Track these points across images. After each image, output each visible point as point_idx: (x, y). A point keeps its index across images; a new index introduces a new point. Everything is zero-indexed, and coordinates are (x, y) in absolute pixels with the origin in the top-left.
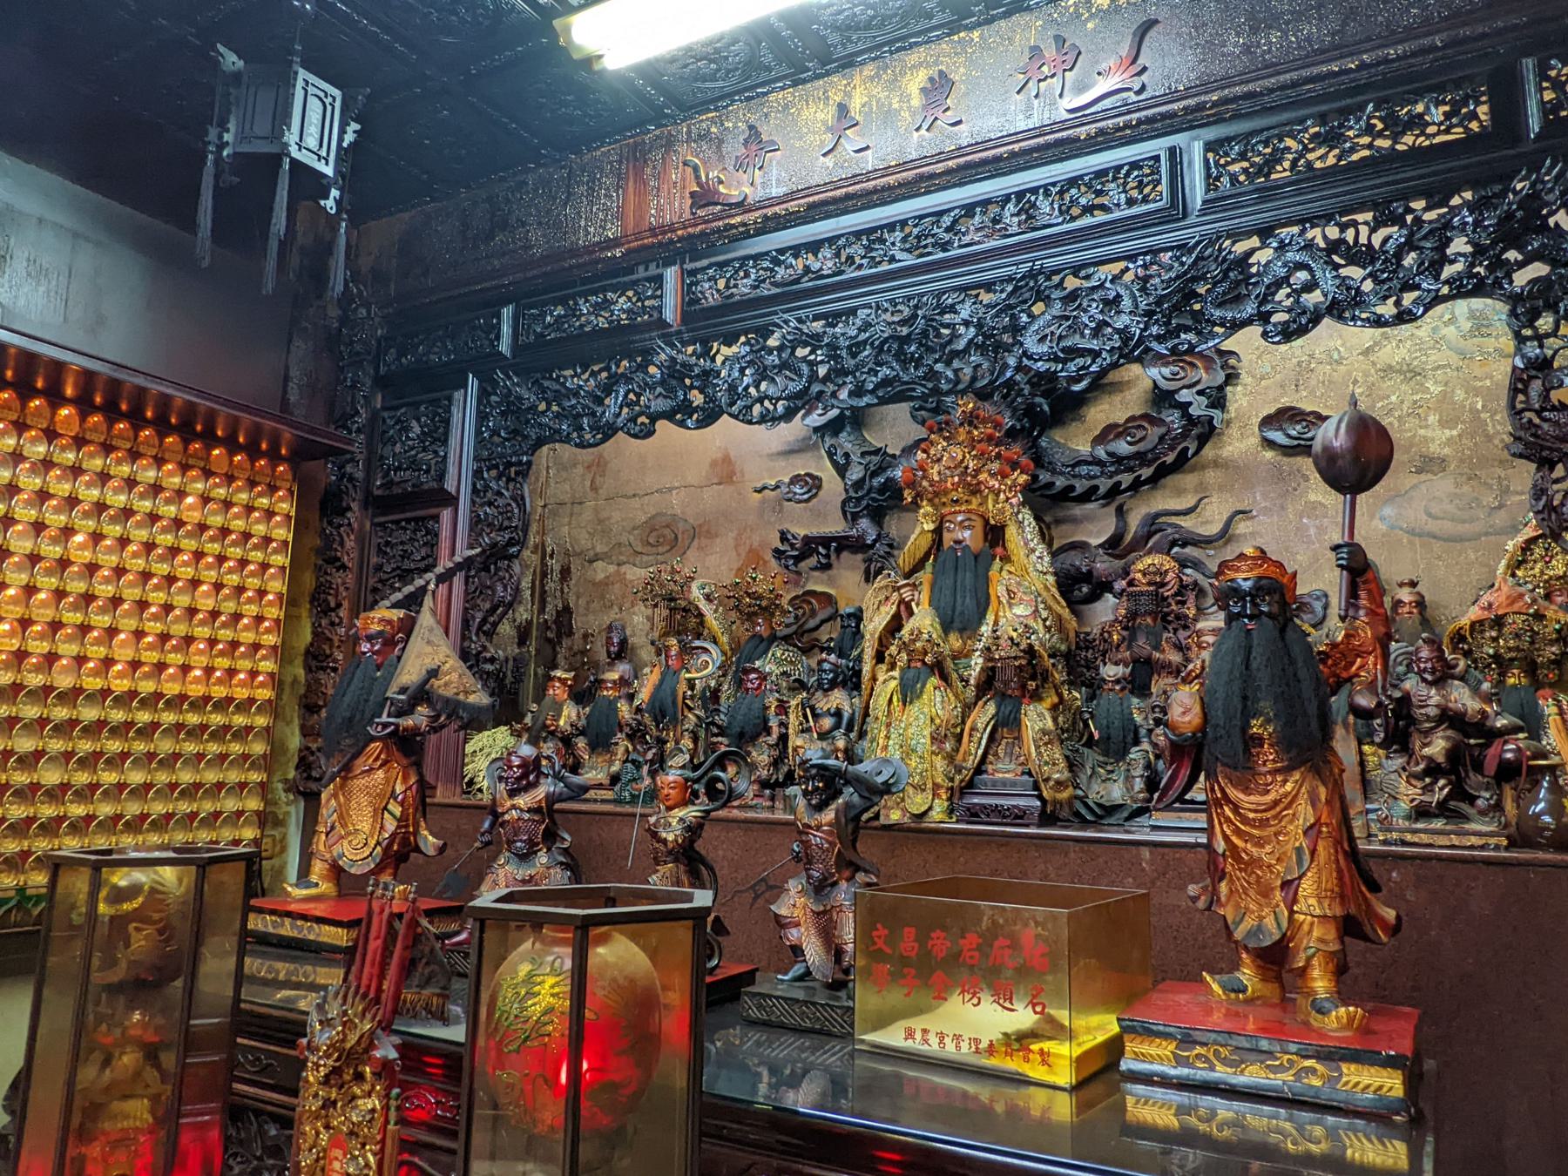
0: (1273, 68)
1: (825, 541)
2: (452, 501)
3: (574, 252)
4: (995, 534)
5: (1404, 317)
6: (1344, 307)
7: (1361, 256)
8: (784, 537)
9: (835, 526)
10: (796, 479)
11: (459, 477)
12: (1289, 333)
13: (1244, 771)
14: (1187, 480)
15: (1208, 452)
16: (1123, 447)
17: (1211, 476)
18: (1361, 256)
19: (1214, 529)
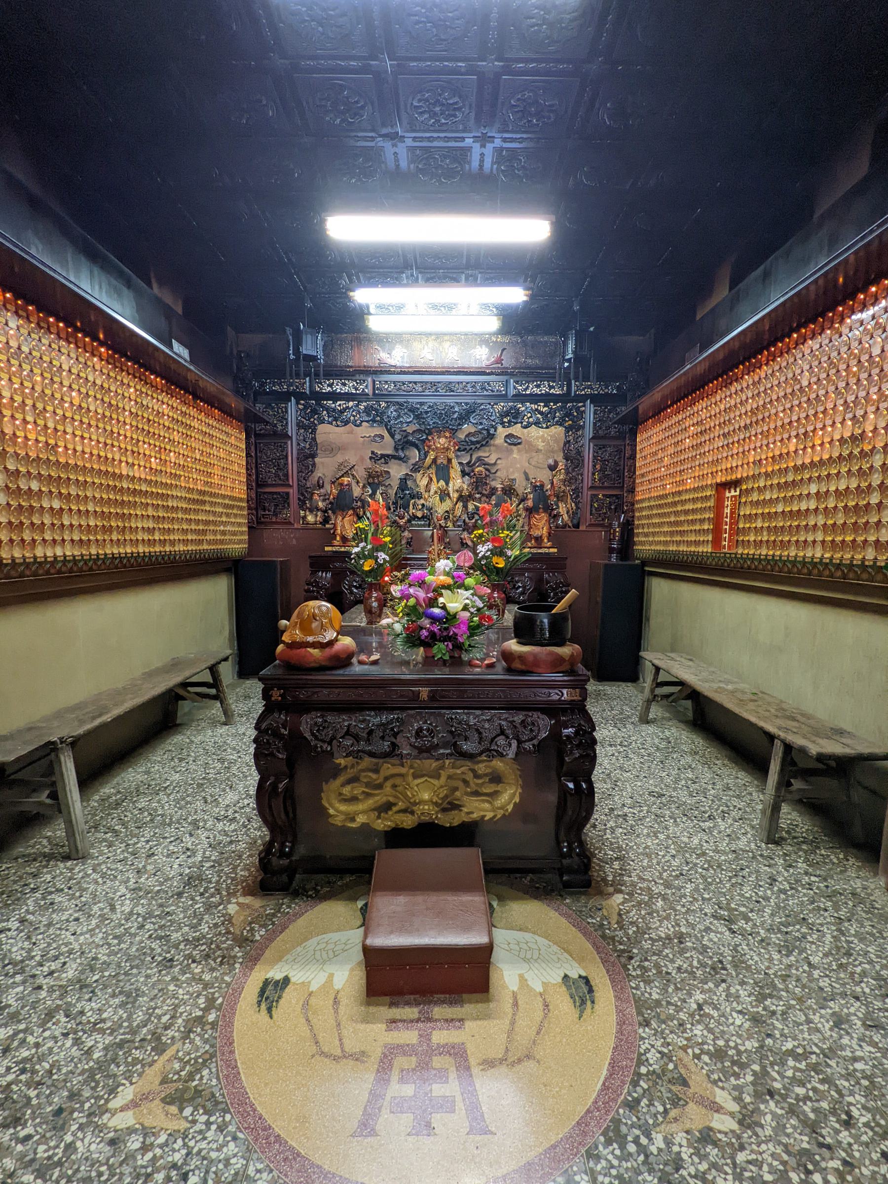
0: (529, 368)
1: (388, 456)
2: (291, 438)
3: (336, 366)
4: (449, 461)
5: (547, 427)
6: (537, 423)
7: (541, 413)
8: (373, 453)
9: (390, 451)
10: (376, 436)
11: (292, 430)
12: (526, 427)
13: (538, 513)
14: (487, 449)
15: (492, 442)
16: (474, 439)
17: (492, 448)
18: (541, 413)
19: (493, 462)
